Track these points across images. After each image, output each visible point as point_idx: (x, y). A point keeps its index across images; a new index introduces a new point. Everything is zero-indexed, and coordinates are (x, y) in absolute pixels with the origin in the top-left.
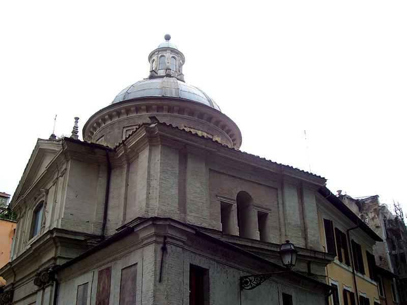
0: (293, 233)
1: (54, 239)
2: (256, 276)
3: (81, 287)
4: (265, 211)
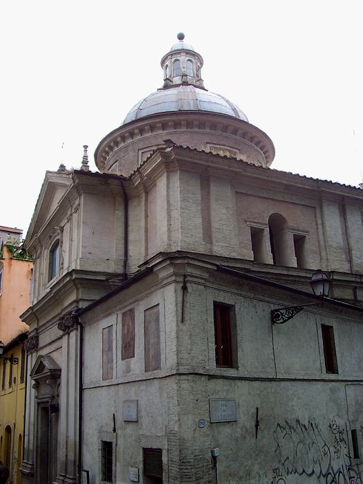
0: (336, 257)
1: (74, 280)
2: (287, 309)
3: (106, 330)
4: (302, 234)
